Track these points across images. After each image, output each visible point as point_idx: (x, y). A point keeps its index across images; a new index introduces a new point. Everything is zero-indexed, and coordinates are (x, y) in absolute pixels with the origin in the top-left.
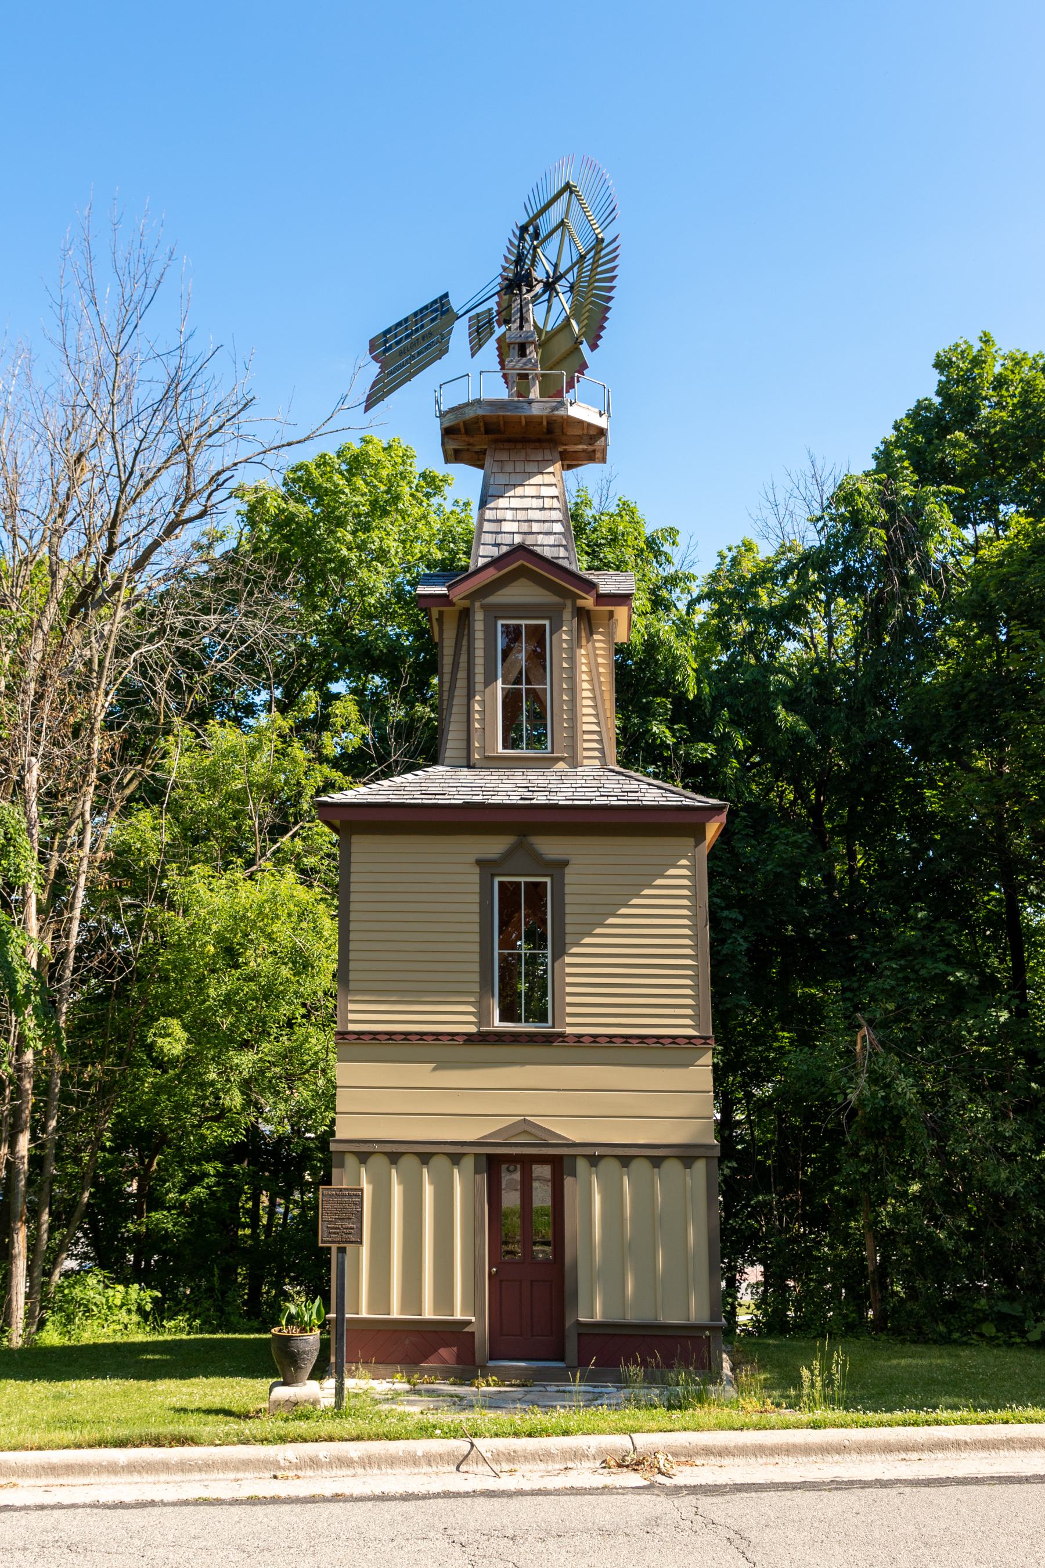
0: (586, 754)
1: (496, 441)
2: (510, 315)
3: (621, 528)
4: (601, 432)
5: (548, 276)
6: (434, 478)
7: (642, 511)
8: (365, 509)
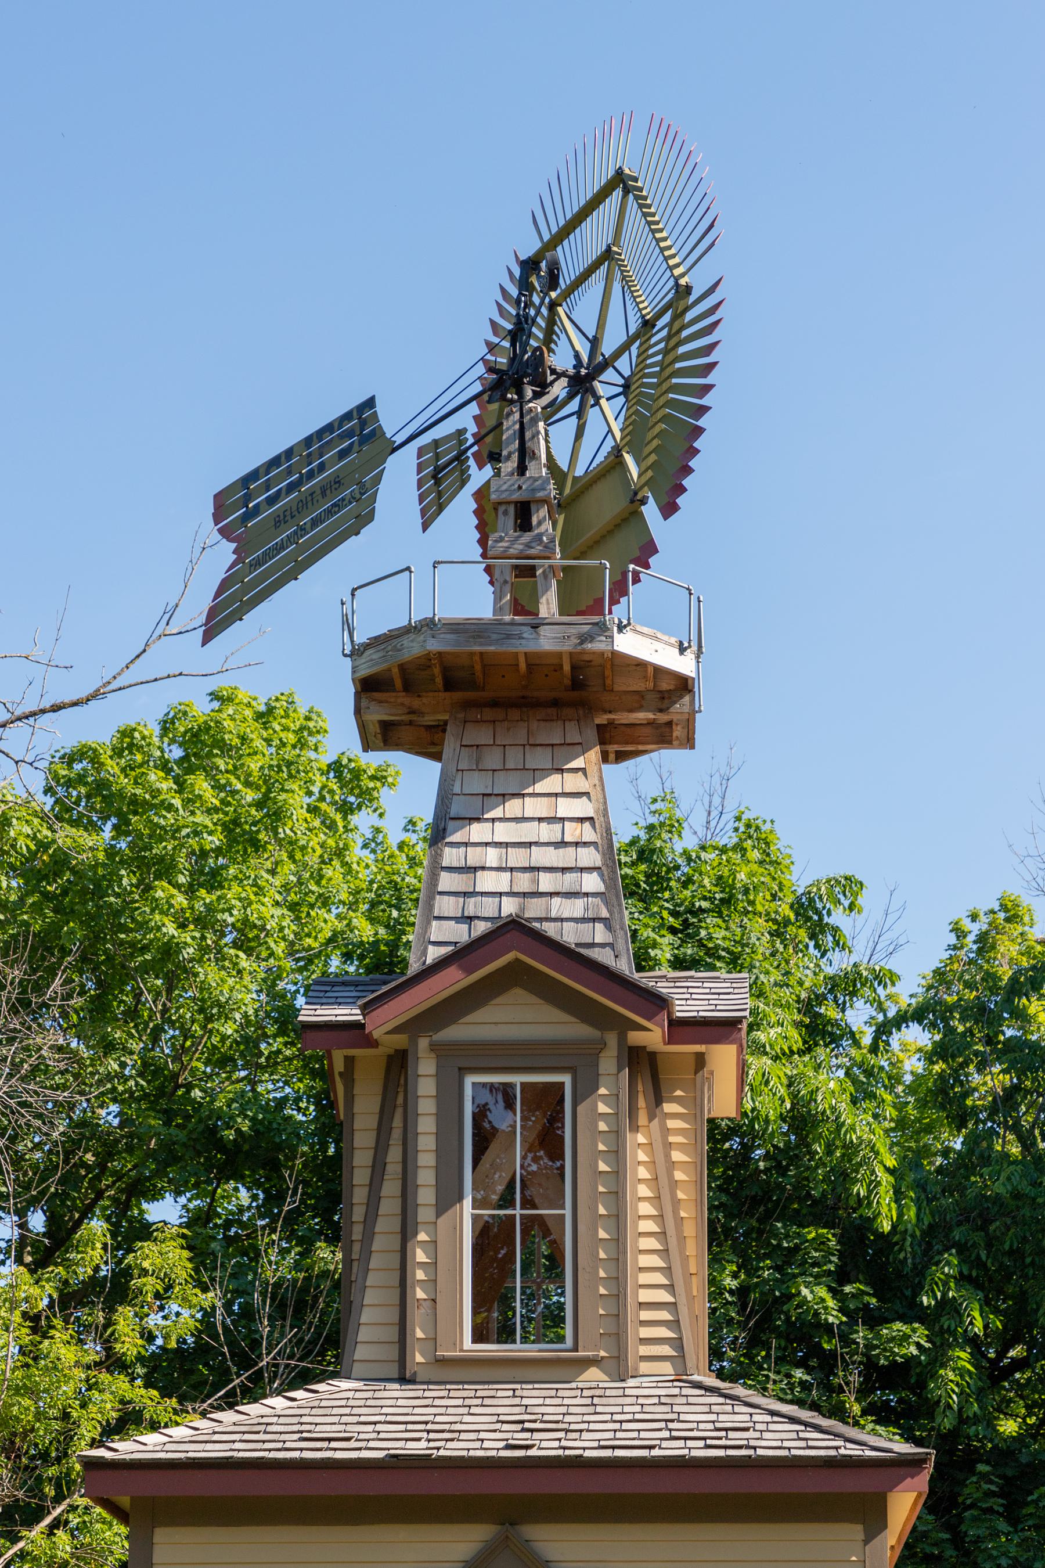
0: (644, 1350)
1: (467, 705)
2: (499, 442)
3: (742, 876)
4: (684, 685)
5: (579, 364)
6: (357, 774)
7: (786, 840)
8: (213, 841)
